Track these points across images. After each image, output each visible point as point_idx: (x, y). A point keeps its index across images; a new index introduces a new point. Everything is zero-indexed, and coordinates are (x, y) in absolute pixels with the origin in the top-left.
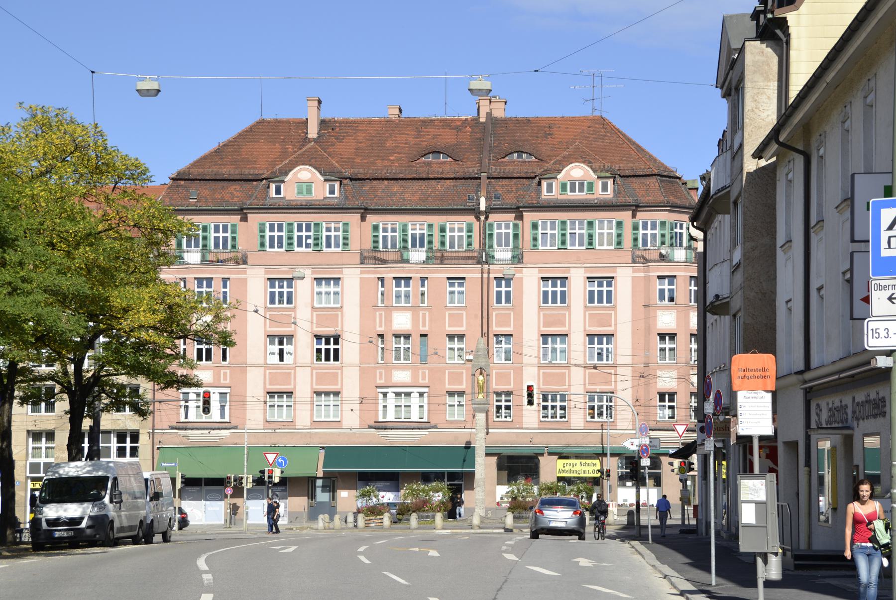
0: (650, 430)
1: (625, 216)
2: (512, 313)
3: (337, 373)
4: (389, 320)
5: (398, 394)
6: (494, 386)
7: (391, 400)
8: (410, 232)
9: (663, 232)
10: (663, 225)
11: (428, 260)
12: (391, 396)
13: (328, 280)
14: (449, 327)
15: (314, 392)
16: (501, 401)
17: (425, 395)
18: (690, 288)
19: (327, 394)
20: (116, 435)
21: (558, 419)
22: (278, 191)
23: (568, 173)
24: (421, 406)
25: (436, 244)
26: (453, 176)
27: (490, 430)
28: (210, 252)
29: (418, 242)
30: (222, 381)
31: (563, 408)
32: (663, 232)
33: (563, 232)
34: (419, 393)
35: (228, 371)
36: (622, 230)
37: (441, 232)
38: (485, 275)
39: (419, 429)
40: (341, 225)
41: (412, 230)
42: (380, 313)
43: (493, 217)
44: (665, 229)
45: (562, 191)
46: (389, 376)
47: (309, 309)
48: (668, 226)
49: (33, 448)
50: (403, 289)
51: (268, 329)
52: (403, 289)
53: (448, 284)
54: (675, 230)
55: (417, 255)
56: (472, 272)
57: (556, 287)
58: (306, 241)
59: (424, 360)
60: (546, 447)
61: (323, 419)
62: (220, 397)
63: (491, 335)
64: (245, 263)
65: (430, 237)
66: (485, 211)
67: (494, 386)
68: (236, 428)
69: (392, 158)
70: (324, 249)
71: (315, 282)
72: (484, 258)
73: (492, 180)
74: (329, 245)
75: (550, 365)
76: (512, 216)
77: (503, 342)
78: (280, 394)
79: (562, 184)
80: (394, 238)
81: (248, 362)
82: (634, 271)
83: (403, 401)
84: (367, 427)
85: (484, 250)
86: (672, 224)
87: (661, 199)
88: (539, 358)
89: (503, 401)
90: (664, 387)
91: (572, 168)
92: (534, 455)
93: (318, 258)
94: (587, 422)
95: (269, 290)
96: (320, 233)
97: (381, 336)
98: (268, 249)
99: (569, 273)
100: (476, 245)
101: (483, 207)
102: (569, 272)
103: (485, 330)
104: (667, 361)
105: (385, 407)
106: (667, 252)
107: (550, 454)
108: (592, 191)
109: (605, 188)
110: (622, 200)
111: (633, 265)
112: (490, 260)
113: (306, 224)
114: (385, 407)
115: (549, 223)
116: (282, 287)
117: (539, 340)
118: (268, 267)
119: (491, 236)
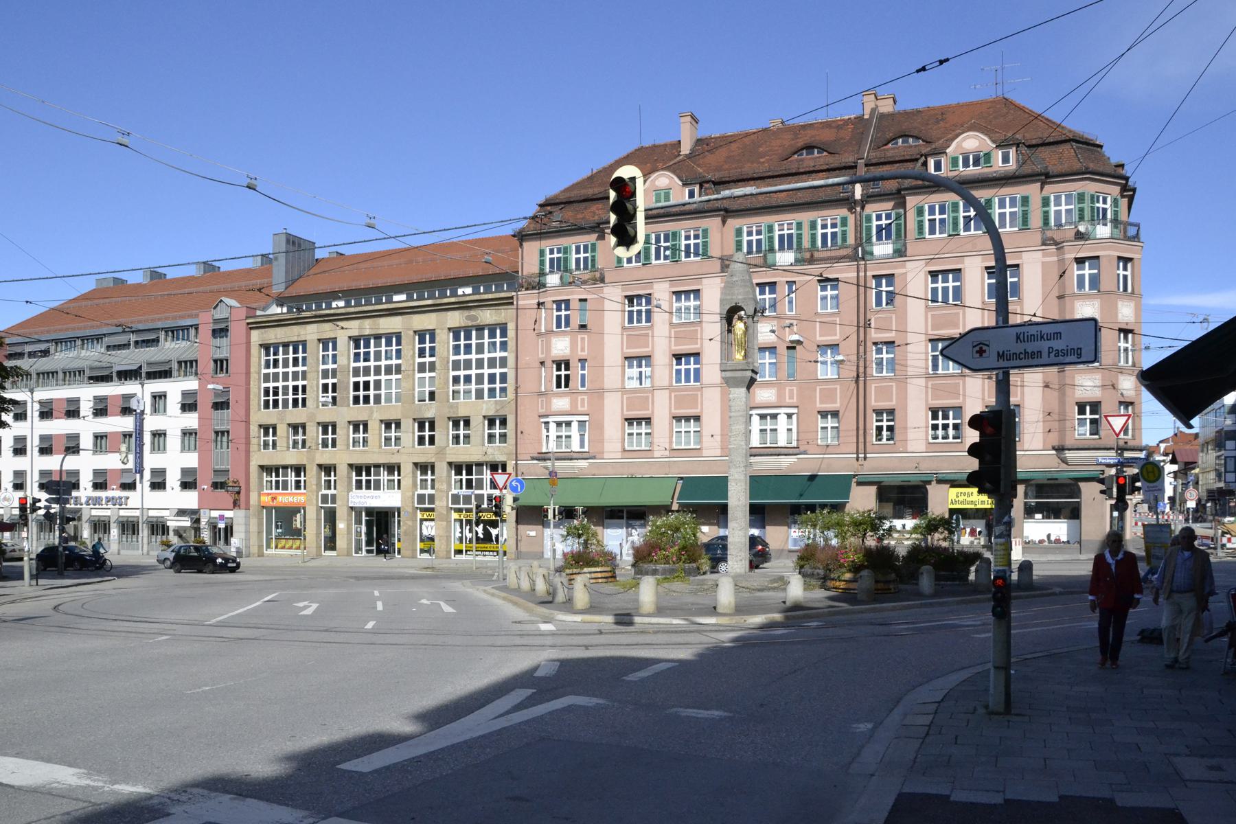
0: (751, 456)
1: (1032, 190)
2: (894, 316)
3: (697, 395)
4: (548, 348)
5: (763, 417)
6: (873, 403)
7: (756, 422)
8: (777, 233)
9: (1080, 205)
10: (1081, 197)
11: (798, 261)
12: (553, 426)
13: (687, 293)
14: (820, 336)
15: (674, 417)
16: (882, 421)
17: (794, 417)
18: (1118, 272)
19: (687, 419)
20: (489, 467)
21: (940, 440)
22: (938, 166)
23: (959, 146)
24: (789, 430)
25: (806, 243)
26: (825, 167)
27: (868, 455)
28: (1051, 229)
29: (787, 243)
30: (580, 409)
31: (890, 429)
32: (1080, 205)
33: (955, 214)
34: (786, 414)
35: (586, 398)
36: (1028, 206)
37: (918, 216)
38: (862, 274)
39: (786, 455)
40: (700, 233)
41: (779, 230)
42: (583, 336)
43: (871, 209)
44: (1084, 203)
45: (953, 167)
46: (549, 403)
47: (668, 326)
48: (1087, 198)
49: (421, 480)
50: (829, 293)
51: (625, 350)
52: (829, 293)
53: (819, 287)
54: (1097, 205)
55: (785, 258)
56: (846, 272)
57: (948, 282)
58: (664, 252)
59: (792, 376)
60: (935, 474)
61: (683, 447)
62: (579, 425)
63: (869, 344)
64: (602, 280)
65: (799, 236)
66: (861, 200)
67: (873, 403)
68: (594, 458)
69: (762, 160)
70: (683, 259)
71: (674, 297)
72: (859, 254)
73: (872, 168)
74: (688, 255)
75: (936, 376)
76: (889, 205)
77: (884, 351)
78: (639, 420)
79: (952, 158)
80: (759, 242)
81: (606, 387)
82: (1044, 256)
83: (769, 426)
84: (1051, 448)
85: (861, 245)
86: (1092, 196)
87: (1077, 166)
88: (927, 369)
89: (885, 420)
90: (1082, 396)
91: (656, 178)
92: (921, 483)
93: (675, 270)
94: (929, 443)
95: (931, 286)
96: (677, 242)
97: (542, 363)
98: (927, 236)
99: (652, 289)
100: (851, 240)
101: (858, 195)
102: (1021, 258)
103: (862, 338)
104: (884, 374)
105: (547, 436)
106: (1087, 229)
107: (940, 482)
108: (990, 163)
109: (1006, 159)
110: (1027, 169)
111: (1044, 247)
112: (867, 257)
113: (664, 235)
114: (547, 436)
115: (1008, 200)
116: (947, 281)
117: (927, 347)
118: (625, 284)
119: (869, 229)
